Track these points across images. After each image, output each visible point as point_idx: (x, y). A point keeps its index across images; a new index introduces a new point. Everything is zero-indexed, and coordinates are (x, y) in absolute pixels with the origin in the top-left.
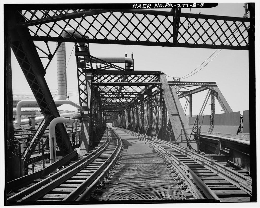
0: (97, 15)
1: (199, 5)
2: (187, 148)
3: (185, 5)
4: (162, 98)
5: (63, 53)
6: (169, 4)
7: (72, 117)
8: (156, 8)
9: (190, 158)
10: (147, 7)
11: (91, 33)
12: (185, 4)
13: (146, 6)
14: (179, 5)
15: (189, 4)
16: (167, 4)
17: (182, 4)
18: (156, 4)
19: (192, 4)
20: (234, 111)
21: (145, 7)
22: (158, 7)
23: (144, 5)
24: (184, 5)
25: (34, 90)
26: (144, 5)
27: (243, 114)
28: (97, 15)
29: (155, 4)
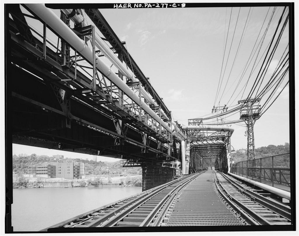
0: (25, 16)
1: (154, 5)
2: (160, 124)
3: (164, 5)
4: (284, 185)
5: (238, 164)
6: (148, 4)
7: (71, 28)
8: (135, 8)
9: (116, 74)
10: (128, 7)
11: (268, 53)
12: (164, 3)
13: (127, 5)
14: (157, 5)
15: (169, 4)
16: (146, 4)
17: (161, 4)
18: (135, 5)
19: (172, 4)
20: (277, 146)
21: (126, 7)
22: (137, 7)
23: (125, 5)
24: (163, 5)
25: (68, 22)
26: (125, 5)
27: (290, 152)
28: (25, 16)
29: (134, 4)
